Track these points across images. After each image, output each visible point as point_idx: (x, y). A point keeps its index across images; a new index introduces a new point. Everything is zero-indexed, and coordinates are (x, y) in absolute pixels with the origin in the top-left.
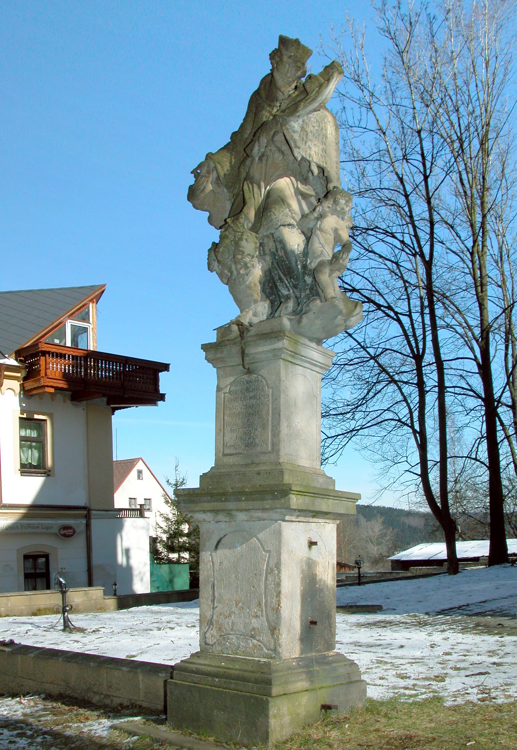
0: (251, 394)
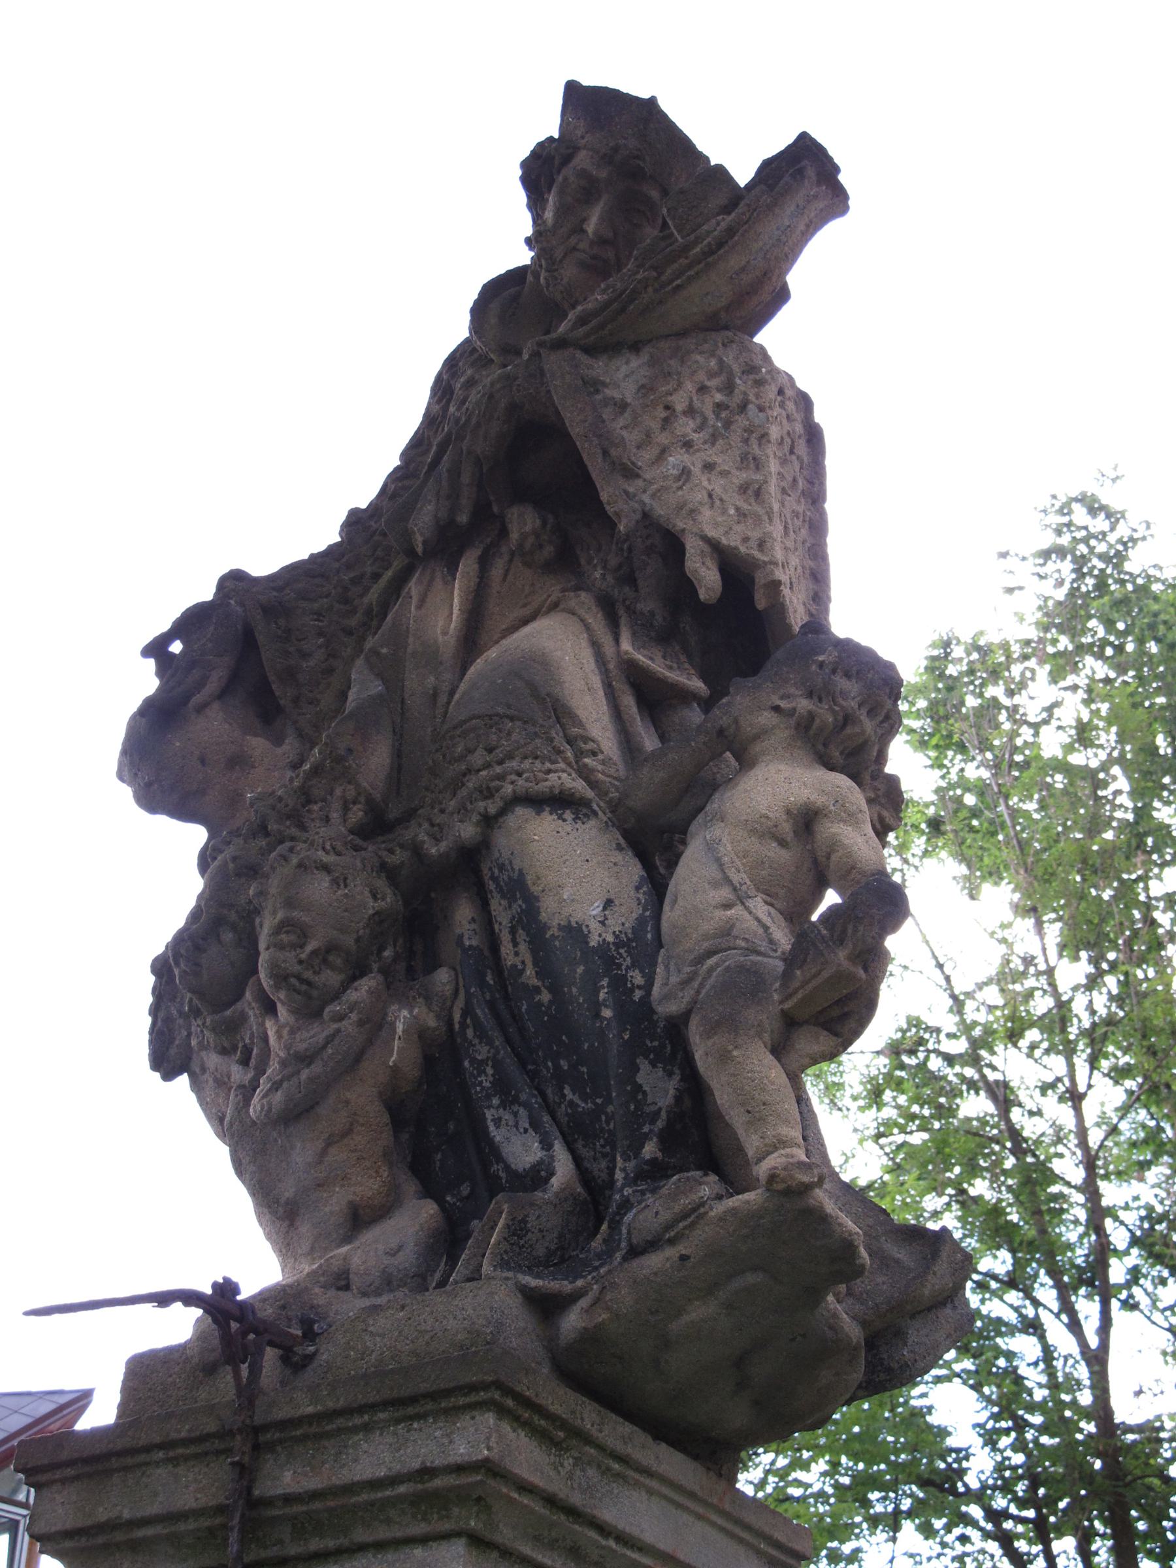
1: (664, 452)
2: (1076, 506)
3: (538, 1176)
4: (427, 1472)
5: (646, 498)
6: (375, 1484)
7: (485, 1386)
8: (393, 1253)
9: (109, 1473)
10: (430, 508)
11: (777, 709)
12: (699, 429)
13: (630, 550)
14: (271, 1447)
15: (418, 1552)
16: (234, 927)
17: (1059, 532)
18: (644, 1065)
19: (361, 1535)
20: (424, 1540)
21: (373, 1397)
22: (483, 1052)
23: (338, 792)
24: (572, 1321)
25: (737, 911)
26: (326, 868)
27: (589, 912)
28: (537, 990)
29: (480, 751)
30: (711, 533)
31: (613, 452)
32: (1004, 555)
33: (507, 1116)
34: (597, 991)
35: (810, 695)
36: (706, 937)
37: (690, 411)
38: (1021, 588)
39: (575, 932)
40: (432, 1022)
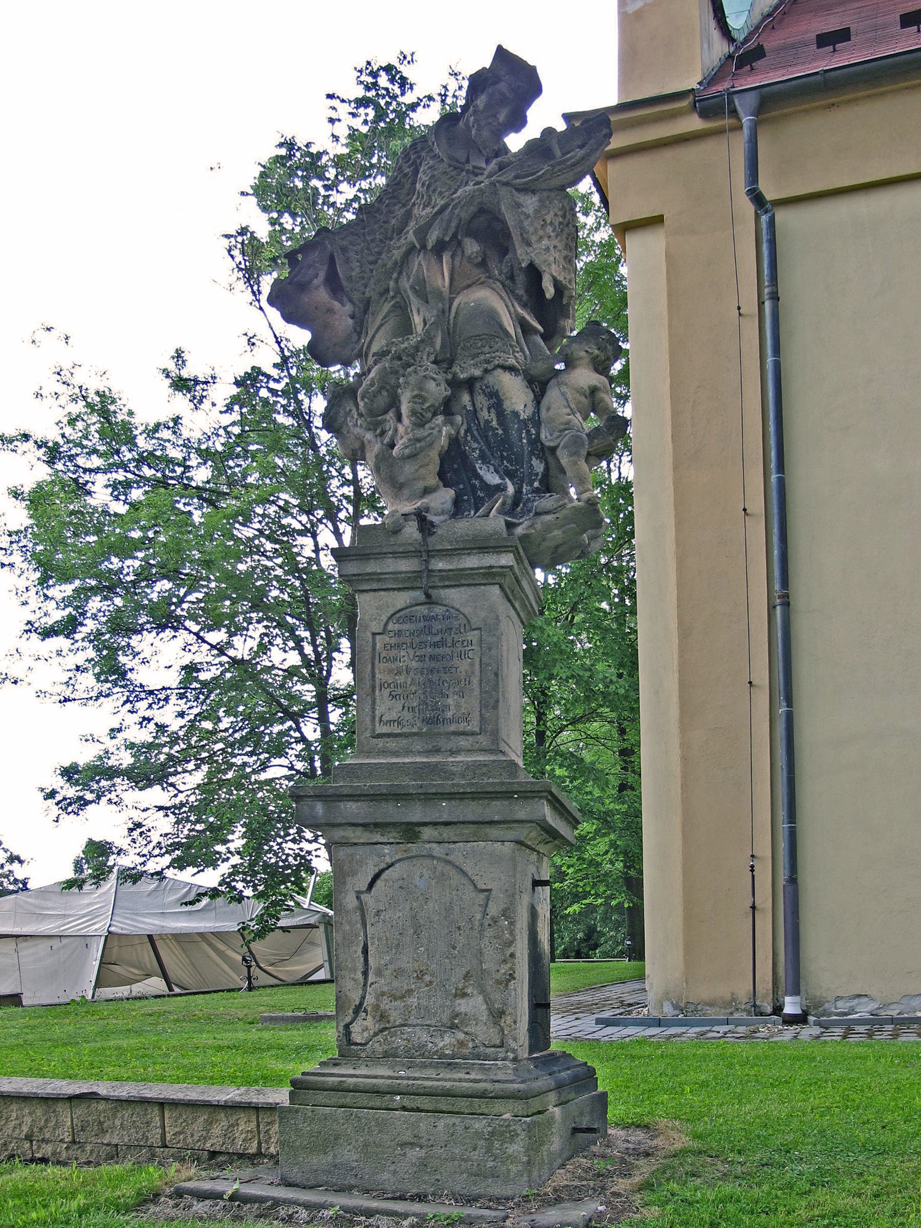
0: (438, 638)
1: (541, 238)
2: (382, 73)
3: (501, 488)
4: (491, 567)
5: (533, 255)
6: (471, 569)
7: (511, 546)
8: (443, 504)
9: (370, 559)
10: (436, 232)
11: (587, 351)
12: (553, 231)
13: (512, 266)
14: (433, 556)
15: (483, 587)
16: (388, 391)
17: (368, 88)
18: (534, 459)
19: (463, 582)
20: (485, 585)
21: (473, 546)
22: (475, 445)
23: (427, 350)
24: (519, 531)
25: (571, 417)
26: (434, 379)
27: (520, 408)
28: (497, 429)
29: (487, 348)
30: (554, 274)
31: (525, 235)
32: (330, 96)
33: (484, 467)
34: (522, 433)
35: (599, 349)
36: (562, 423)
37: (551, 224)
38: (339, 120)
39: (516, 414)
40: (453, 432)
